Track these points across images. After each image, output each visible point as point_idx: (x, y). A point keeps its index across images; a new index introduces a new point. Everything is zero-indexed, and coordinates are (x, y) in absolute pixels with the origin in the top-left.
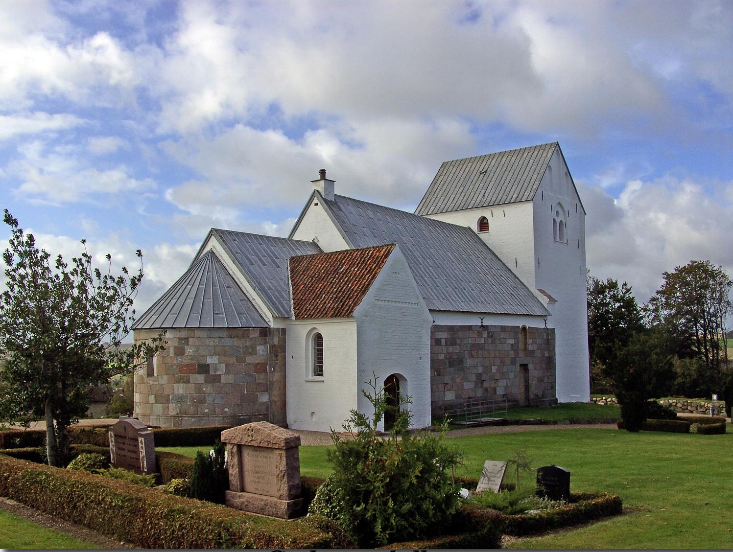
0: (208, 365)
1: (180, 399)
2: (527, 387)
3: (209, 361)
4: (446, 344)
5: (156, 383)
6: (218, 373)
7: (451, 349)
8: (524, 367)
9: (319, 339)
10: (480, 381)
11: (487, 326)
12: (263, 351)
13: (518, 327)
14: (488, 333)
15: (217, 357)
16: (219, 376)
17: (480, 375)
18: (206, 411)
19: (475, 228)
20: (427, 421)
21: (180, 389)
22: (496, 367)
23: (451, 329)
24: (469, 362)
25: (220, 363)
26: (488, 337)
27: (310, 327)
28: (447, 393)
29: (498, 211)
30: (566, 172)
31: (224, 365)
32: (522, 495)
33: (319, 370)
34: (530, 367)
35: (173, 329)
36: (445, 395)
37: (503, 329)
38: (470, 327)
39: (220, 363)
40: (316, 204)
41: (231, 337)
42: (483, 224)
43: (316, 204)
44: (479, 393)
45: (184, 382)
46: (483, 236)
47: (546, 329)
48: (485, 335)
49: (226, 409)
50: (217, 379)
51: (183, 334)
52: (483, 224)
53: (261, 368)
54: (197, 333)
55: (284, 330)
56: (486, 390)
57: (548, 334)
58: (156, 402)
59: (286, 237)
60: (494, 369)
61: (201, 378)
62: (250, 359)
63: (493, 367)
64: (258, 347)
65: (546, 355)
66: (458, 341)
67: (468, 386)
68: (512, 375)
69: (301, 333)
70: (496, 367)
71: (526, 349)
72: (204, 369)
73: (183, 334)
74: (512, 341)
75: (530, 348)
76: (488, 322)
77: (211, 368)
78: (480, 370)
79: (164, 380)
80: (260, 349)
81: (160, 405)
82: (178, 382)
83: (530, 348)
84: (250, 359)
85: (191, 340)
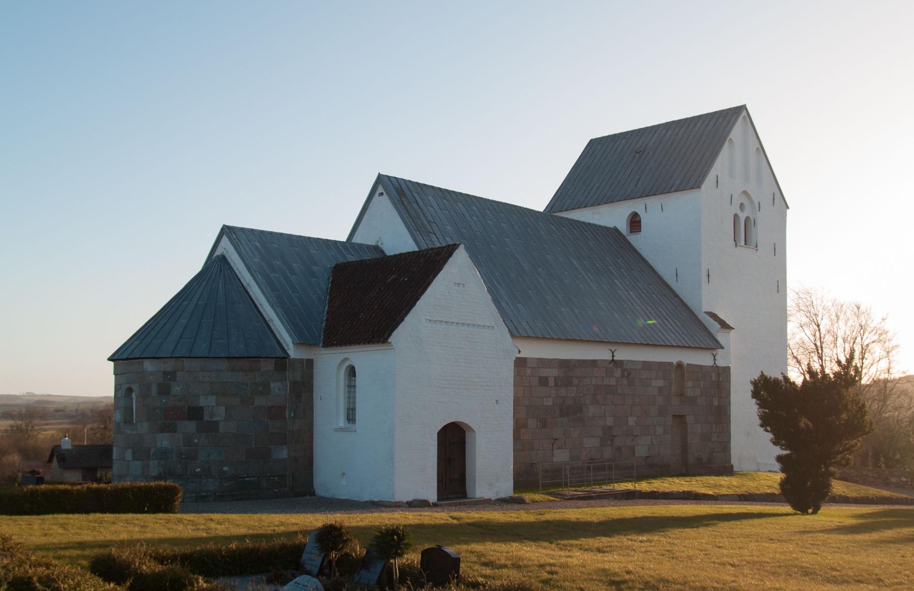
0: (202, 408)
1: (163, 454)
2: (685, 448)
3: (202, 402)
4: (556, 385)
5: (134, 432)
6: (216, 419)
7: (563, 392)
8: (680, 418)
9: (352, 372)
10: (608, 436)
11: (622, 362)
12: (279, 390)
13: (670, 364)
14: (623, 371)
15: (214, 397)
16: (217, 423)
17: (610, 428)
18: (198, 470)
19: (623, 227)
20: (506, 488)
21: (164, 441)
22: (635, 419)
23: (564, 364)
24: (591, 410)
25: (218, 405)
26: (623, 376)
27: (342, 357)
28: (556, 452)
29: (653, 202)
30: (757, 149)
31: (224, 408)
32: (300, 536)
33: (351, 416)
34: (690, 419)
35: (157, 360)
36: (553, 455)
37: (647, 365)
38: (594, 363)
39: (218, 405)
40: (382, 194)
41: (233, 370)
42: (635, 223)
43: (382, 194)
44: (608, 453)
45: (169, 432)
46: (633, 239)
47: (715, 368)
48: (618, 373)
49: (225, 469)
50: (213, 427)
51: (170, 365)
52: (635, 223)
53: (276, 413)
54: (187, 363)
55: (310, 363)
56: (619, 449)
57: (718, 374)
58: (134, 459)
59: (344, 238)
60: (632, 421)
61: (190, 426)
62: (260, 401)
63: (630, 419)
64: (272, 385)
65: (716, 403)
66: (575, 381)
67: (591, 443)
68: (660, 431)
69: (329, 363)
70: (635, 419)
71: (681, 395)
72: (195, 413)
73: (170, 365)
74: (660, 383)
75: (689, 393)
76: (623, 354)
77: (206, 413)
78: (610, 421)
79: (144, 428)
80: (275, 386)
81: (139, 463)
82: (162, 431)
83: (689, 393)
84: (260, 401)
85: (179, 374)
